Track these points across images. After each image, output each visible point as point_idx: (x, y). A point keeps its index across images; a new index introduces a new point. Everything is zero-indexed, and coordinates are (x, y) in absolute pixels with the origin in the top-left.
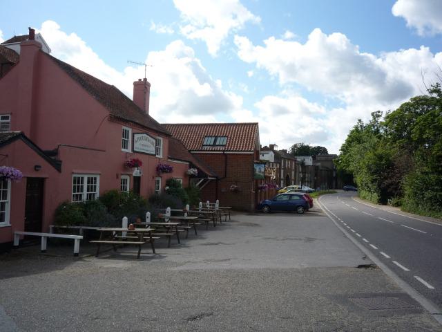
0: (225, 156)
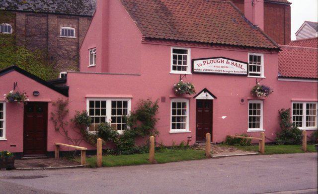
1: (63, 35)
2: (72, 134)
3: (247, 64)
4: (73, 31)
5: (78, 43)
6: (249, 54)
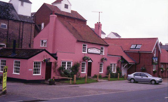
0: (139, 53)
1: (2, 27)
2: (58, 74)
3: (101, 50)
4: (6, 26)
5: (8, 31)
6: (101, 47)
